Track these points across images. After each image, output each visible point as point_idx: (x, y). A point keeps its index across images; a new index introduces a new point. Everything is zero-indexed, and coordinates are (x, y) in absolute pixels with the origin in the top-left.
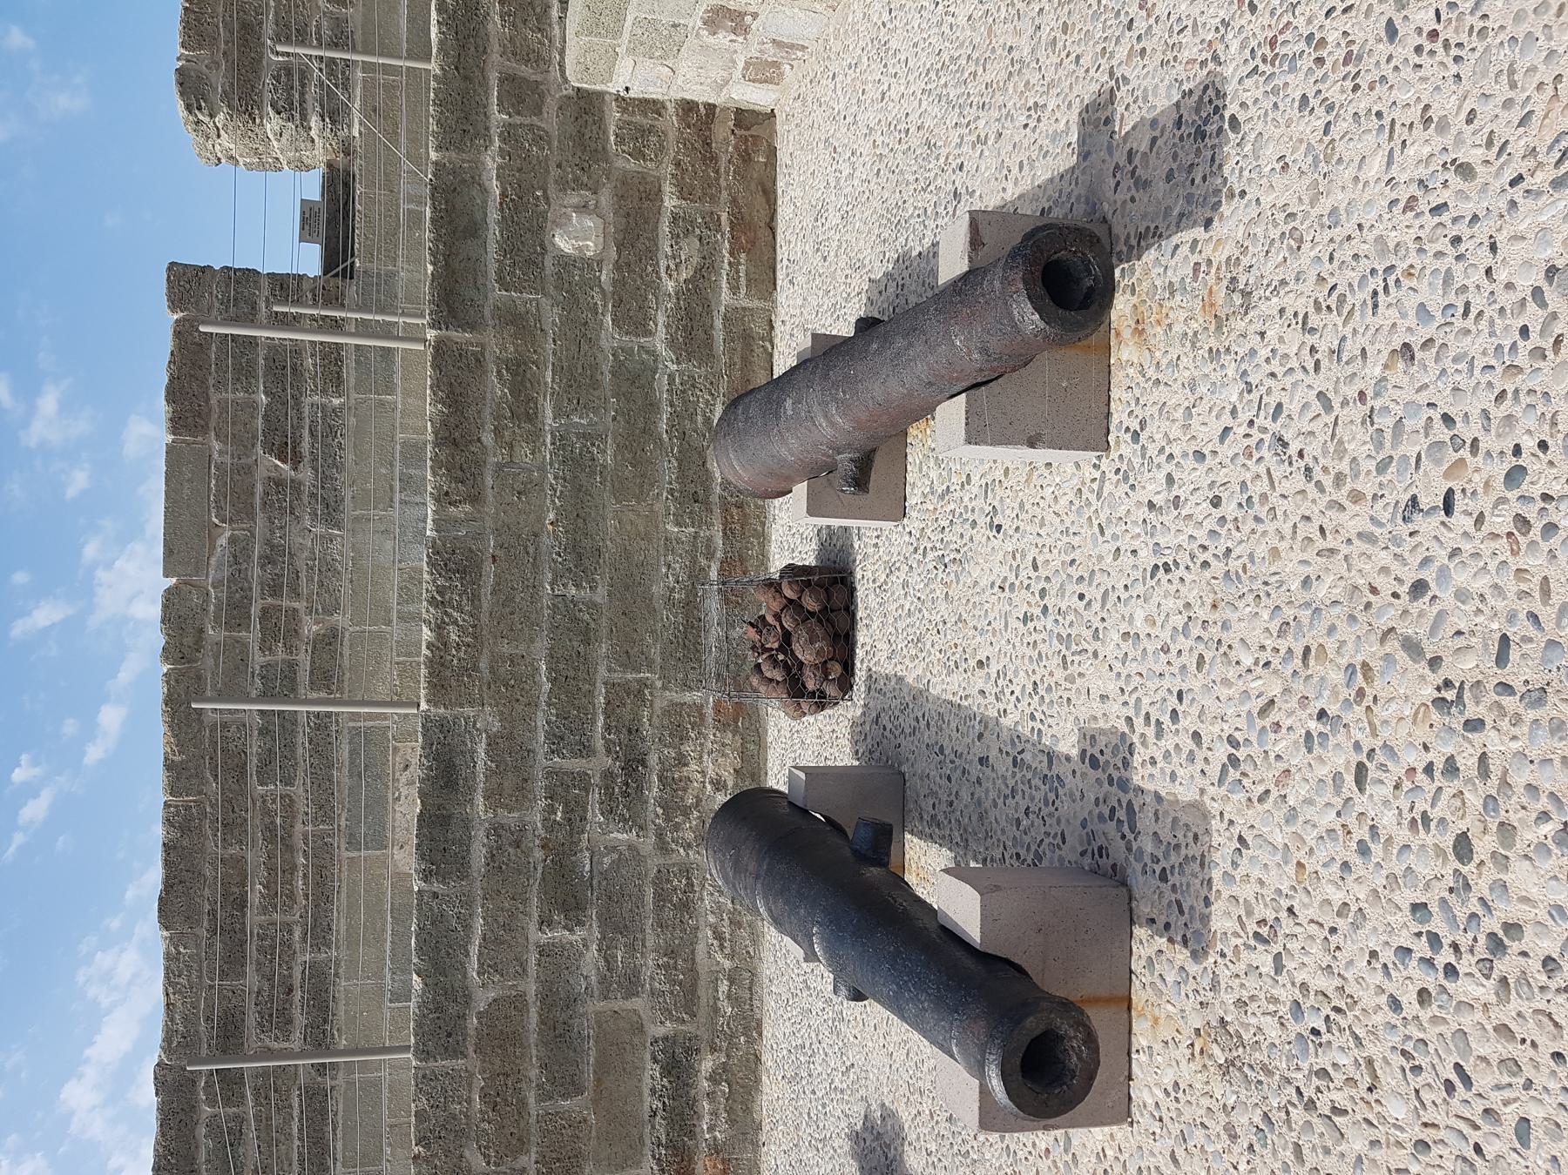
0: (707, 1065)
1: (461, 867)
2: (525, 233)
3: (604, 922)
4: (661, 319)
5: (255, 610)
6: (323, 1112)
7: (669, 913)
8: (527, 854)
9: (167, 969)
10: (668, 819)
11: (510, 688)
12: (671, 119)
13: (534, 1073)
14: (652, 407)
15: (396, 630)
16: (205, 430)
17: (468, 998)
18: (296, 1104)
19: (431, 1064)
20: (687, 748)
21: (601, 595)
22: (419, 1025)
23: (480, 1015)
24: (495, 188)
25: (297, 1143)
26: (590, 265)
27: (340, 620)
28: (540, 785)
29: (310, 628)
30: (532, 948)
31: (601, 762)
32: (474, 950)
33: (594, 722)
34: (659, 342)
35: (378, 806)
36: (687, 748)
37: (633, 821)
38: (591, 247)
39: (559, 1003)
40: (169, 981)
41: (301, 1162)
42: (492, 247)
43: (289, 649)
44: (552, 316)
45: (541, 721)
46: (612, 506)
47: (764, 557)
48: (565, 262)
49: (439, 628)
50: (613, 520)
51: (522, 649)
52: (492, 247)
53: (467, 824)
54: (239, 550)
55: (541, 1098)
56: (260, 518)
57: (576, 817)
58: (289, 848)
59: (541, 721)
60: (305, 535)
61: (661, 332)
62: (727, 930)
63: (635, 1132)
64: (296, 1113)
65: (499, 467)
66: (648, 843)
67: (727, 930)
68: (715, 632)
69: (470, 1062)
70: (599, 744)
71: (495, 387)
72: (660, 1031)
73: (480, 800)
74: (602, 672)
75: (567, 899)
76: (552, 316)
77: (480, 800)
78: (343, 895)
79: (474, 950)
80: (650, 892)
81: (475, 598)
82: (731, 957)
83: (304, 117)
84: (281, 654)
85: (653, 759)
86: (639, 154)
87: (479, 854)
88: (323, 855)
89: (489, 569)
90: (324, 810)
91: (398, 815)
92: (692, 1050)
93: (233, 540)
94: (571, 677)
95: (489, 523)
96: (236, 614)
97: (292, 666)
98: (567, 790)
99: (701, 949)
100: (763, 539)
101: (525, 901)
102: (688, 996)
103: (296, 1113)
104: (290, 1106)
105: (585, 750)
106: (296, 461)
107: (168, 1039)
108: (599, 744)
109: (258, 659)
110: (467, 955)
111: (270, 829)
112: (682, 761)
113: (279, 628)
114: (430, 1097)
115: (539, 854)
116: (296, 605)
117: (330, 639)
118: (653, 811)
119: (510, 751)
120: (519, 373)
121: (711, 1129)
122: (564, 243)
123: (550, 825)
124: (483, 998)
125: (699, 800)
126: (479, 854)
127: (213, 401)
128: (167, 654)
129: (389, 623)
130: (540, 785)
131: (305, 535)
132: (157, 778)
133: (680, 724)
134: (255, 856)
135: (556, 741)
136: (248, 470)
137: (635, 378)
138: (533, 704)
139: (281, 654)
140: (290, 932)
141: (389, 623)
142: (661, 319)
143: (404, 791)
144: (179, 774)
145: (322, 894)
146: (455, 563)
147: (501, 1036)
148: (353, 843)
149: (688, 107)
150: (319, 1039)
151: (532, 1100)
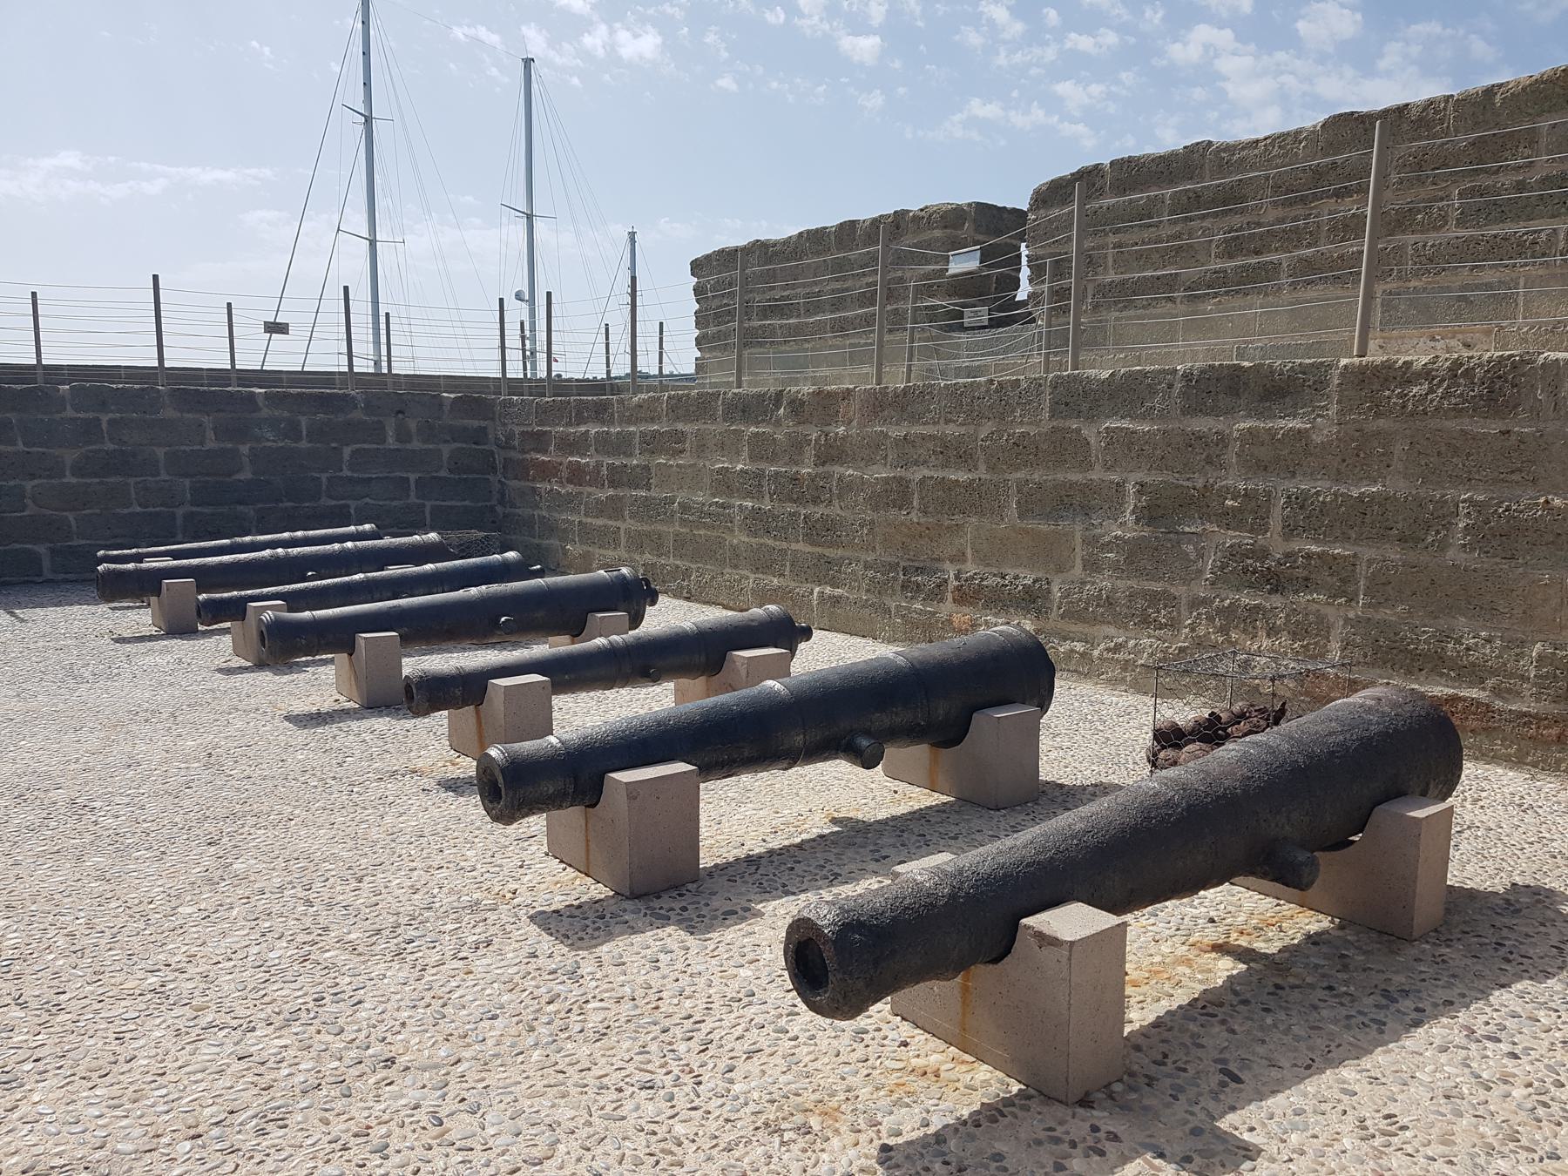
10: (1219, 611)
11: (1357, 454)
19: (1048, 390)
32: (1126, 424)
36: (1285, 639)
45: (1321, 485)
49: (1427, 374)
53: (1230, 412)
55: (1018, 482)
69: (1046, 426)
79: (1126, 424)
98: (1253, 512)
105: (1290, 531)
108: (1295, 546)
112: (1272, 631)
124: (1089, 432)
126: (1202, 424)
133: (1307, 630)
135: (1299, 502)
138: (1339, 478)
147: (1065, 448)
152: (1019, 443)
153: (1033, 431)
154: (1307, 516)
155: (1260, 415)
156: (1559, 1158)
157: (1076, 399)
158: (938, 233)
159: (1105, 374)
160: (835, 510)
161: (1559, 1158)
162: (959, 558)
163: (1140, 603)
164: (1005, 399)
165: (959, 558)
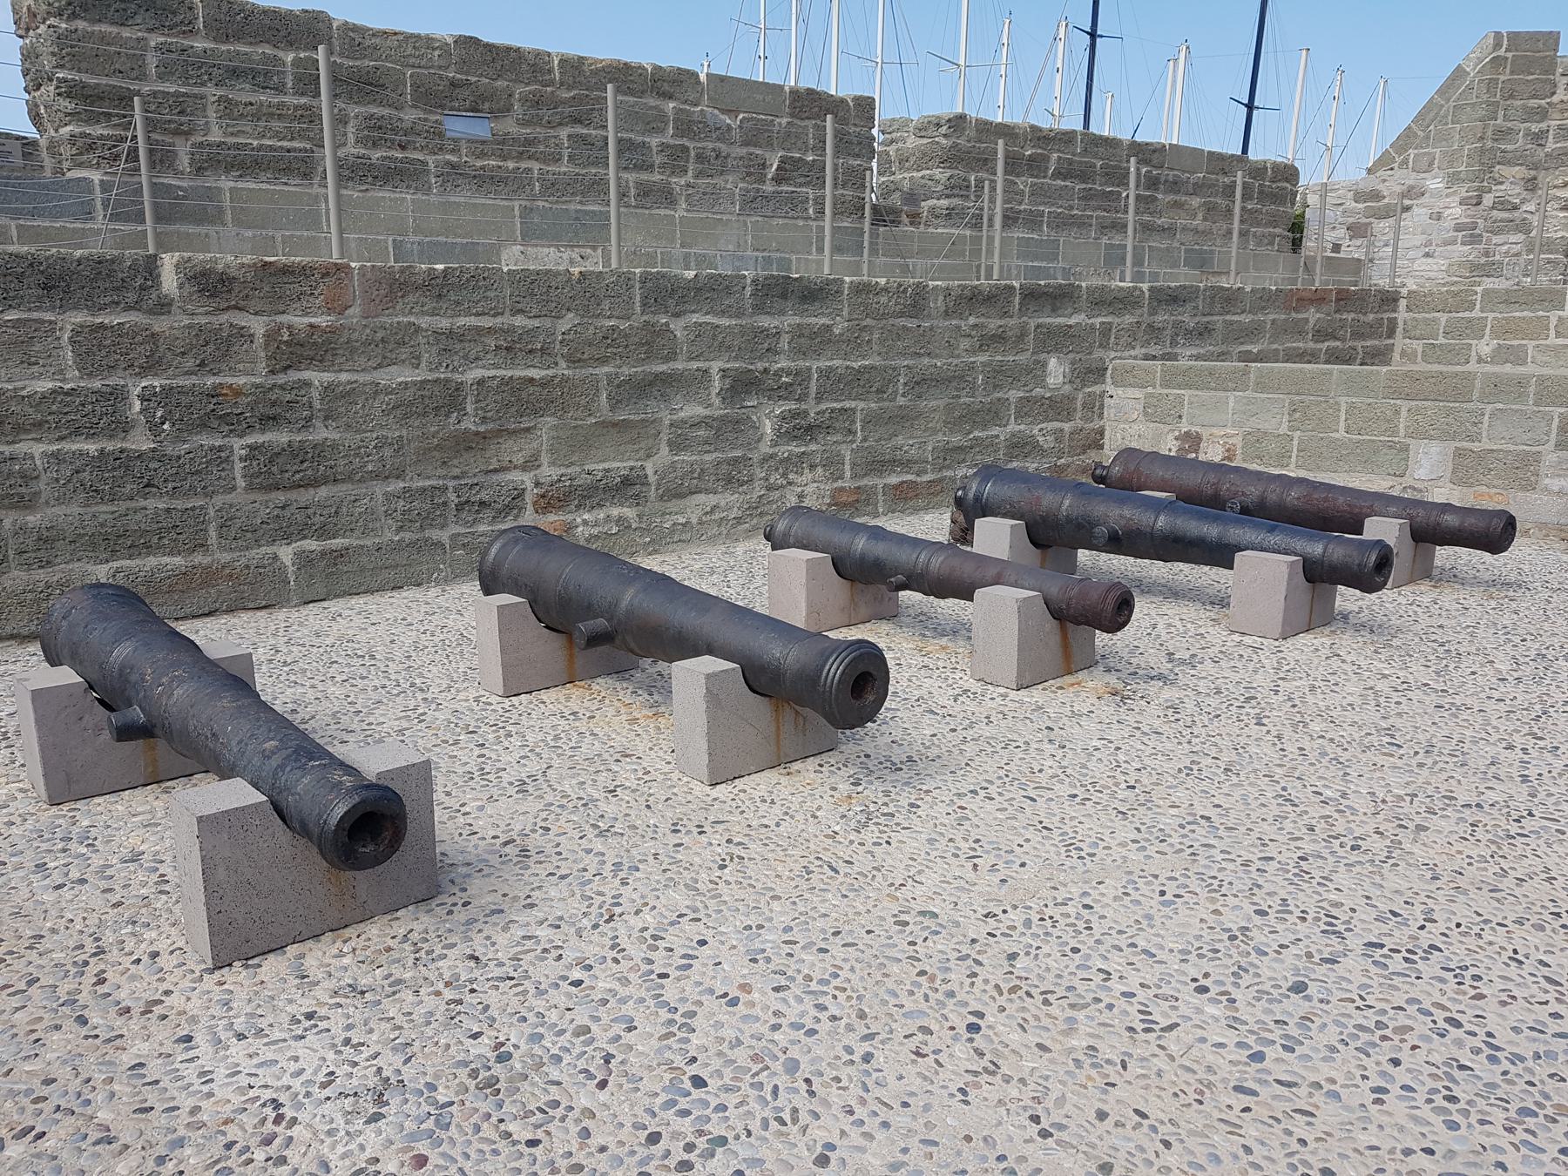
0: (629, 512)
1: (759, 309)
2: (1054, 340)
3: (722, 419)
4: (1022, 427)
5: (685, 142)
6: (288, 171)
7: (725, 468)
8: (760, 358)
9: (418, 36)
10: (781, 461)
11: (854, 342)
12: (1096, 424)
13: (626, 370)
14: (985, 427)
15: (678, 251)
16: (792, 115)
17: (677, 315)
18: (296, 144)
19: (638, 285)
20: (820, 470)
21: (901, 401)
22: (664, 276)
23: (667, 324)
24: (1072, 321)
25: (255, 143)
26: (1041, 381)
27: (681, 211)
28: (802, 364)
29: (678, 182)
30: (707, 364)
31: (813, 409)
32: (709, 319)
33: (836, 401)
34: (1013, 427)
35: (553, 236)
36: (820, 470)
37: (782, 436)
38: (1051, 381)
39: (664, 385)
40: (409, 37)
41: (237, 146)
42: (1049, 320)
43: (663, 166)
44: (1022, 358)
45: (836, 363)
46: (942, 403)
47: (256, 592)
48: (1044, 365)
49: (885, 290)
50: (935, 402)
51: (875, 347)
52: (1049, 320)
53: (782, 313)
54: (723, 133)
55: (608, 375)
56: (744, 151)
57: (782, 392)
58: (520, 156)
59: (836, 363)
60: (732, 183)
61: (1017, 428)
62: (716, 516)
63: (575, 458)
64: (285, 144)
65: (958, 327)
66: (765, 448)
67: (716, 516)
68: (880, 482)
69: (638, 319)
70: (823, 406)
71: (994, 324)
72: (650, 471)
73: (797, 320)
74: (862, 405)
75: (741, 385)
76: (1022, 358)
77: (797, 320)
78: (483, 201)
79: (709, 319)
80: (738, 453)
81: (901, 314)
82: (701, 523)
83: (948, 196)
84: (658, 160)
85: (813, 447)
86: (1084, 406)
87: (765, 322)
88: (517, 183)
89: (911, 323)
90: (552, 187)
91: (546, 250)
92: (638, 499)
93: (729, 127)
94: (857, 382)
95: (935, 322)
96: (686, 126)
97: (650, 168)
98: (793, 387)
99: (701, 498)
100: (331, 578)
101: (736, 358)
102: (675, 493)
103: (285, 144)
104: (292, 139)
105: (819, 399)
106: (778, 180)
107: (355, 28)
108: (823, 406)
109: (654, 141)
110: (707, 313)
111: (529, 142)
112: (812, 467)
113: (676, 158)
114: (615, 283)
115: (760, 366)
116: (690, 173)
117: (668, 198)
118: (785, 450)
119: (817, 341)
120: (999, 338)
121: (585, 523)
122: (1053, 362)
123: (778, 374)
124: (678, 327)
125: (790, 483)
126: (765, 322)
127: (806, 122)
128: (657, 68)
129: (682, 246)
130: (802, 364)
131: (732, 183)
132: (574, 50)
133: (832, 464)
134: (509, 126)
135: (825, 374)
136: (770, 144)
137: (993, 414)
138: (846, 357)
139: (658, 160)
140: (453, 151)
141: (682, 246)
142: (1022, 427)
143: (565, 256)
144: (574, 67)
145: (485, 181)
146: (916, 302)
147: (654, 342)
148: (526, 212)
149: (1101, 433)
150: (351, 172)
151: (606, 369)
152: (610, 336)
153: (624, 325)
154: (833, 383)
155: (801, 314)
156: (54, 1080)
157: (665, 294)
158: (938, 173)
159: (691, 274)
160: (321, 433)
161: (54, 1080)
162: (531, 464)
163: (725, 468)
164: (587, 292)
165: (531, 464)
